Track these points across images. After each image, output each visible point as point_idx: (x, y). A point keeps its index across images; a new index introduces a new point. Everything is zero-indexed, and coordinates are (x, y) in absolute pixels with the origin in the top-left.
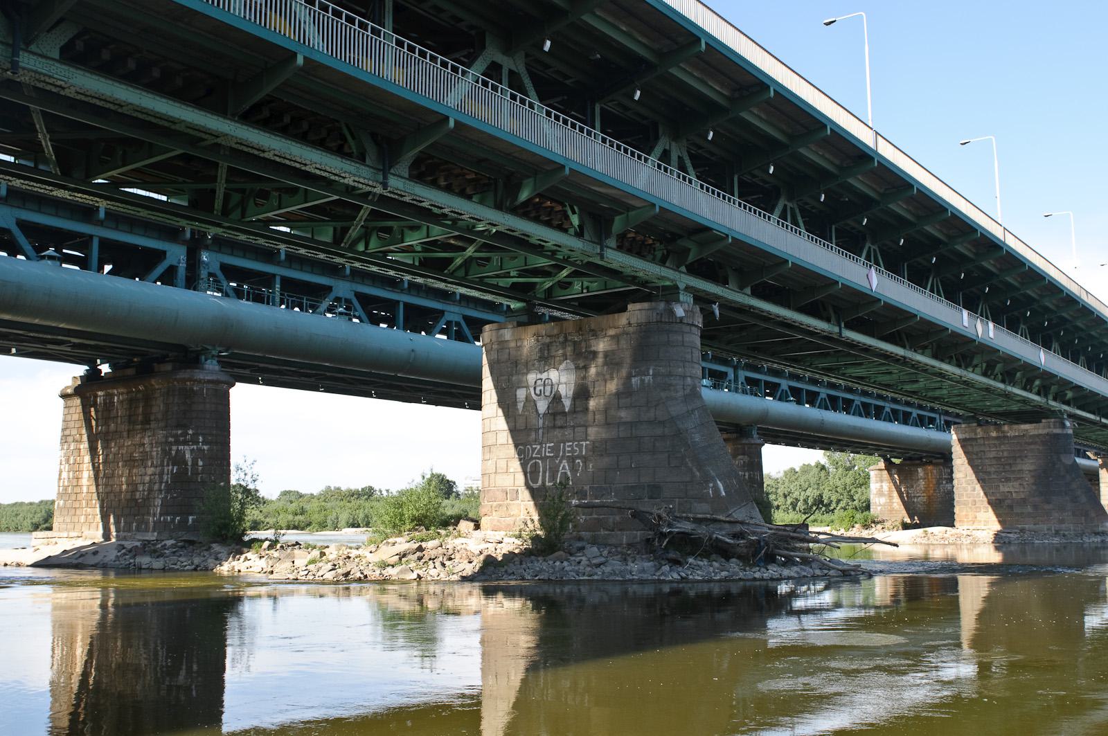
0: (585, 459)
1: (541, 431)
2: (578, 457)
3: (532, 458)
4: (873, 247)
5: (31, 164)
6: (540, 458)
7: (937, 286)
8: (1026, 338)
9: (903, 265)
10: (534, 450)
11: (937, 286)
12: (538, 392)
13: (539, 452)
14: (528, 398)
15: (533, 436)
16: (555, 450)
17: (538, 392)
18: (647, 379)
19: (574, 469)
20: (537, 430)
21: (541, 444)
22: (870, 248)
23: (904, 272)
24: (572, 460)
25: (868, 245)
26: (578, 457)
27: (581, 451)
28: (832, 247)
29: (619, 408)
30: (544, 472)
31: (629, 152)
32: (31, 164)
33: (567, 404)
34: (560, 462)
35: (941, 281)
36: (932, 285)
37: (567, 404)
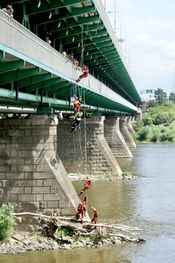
29: (25, 165)
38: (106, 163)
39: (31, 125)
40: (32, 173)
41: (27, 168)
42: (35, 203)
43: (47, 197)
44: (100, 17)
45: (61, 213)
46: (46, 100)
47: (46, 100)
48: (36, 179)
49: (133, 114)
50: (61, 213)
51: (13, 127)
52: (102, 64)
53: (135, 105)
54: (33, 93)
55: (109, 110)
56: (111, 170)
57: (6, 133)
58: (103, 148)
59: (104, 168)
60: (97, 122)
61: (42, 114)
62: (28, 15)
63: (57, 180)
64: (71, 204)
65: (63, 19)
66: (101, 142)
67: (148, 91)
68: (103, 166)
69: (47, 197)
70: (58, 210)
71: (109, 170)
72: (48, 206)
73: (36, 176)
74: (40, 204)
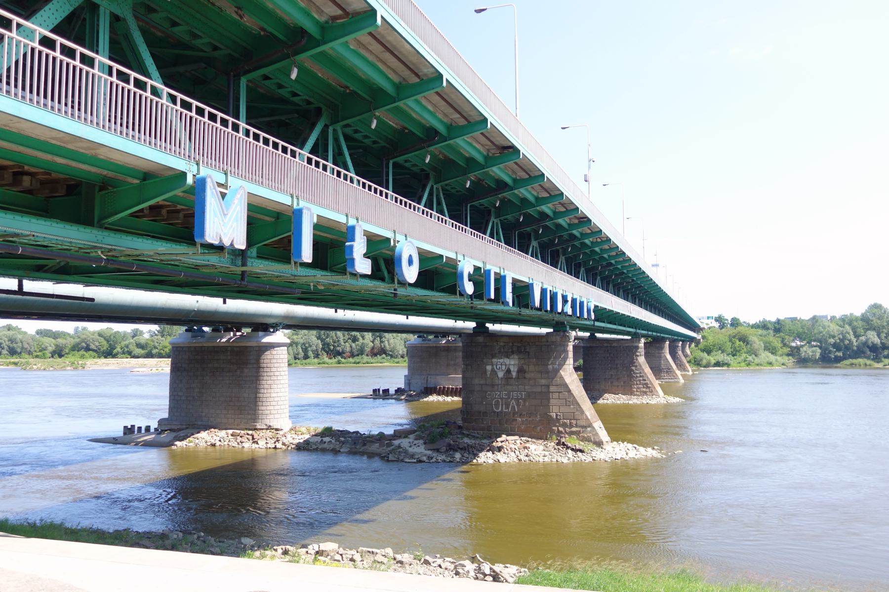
0: (524, 400)
1: (500, 386)
2: (521, 399)
3: (495, 398)
4: (496, 221)
5: (598, 335)
6: (500, 398)
7: (336, 140)
8: (499, 240)
9: (466, 207)
10: (496, 394)
11: (336, 140)
12: (498, 368)
13: (499, 395)
14: (493, 370)
15: (496, 387)
16: (508, 395)
17: (498, 368)
18: (555, 366)
19: (518, 405)
20: (498, 385)
21: (500, 392)
22: (493, 222)
23: (237, 100)
24: (517, 400)
25: (492, 219)
26: (521, 399)
27: (522, 396)
28: (446, 221)
29: (541, 378)
30: (502, 405)
31: (251, 135)
32: (598, 335)
33: (514, 374)
34: (511, 401)
35: (347, 138)
36: (431, 194)
37: (514, 374)
38: (646, 384)
39: (547, 341)
40: (548, 386)
41: (543, 382)
42: (551, 414)
43: (563, 409)
44: (160, 203)
45: (576, 425)
46: (638, 331)
47: (638, 331)
48: (552, 392)
49: (692, 340)
50: (576, 425)
51: (531, 344)
52: (636, 288)
53: (694, 332)
54: (633, 328)
55: (658, 334)
56: (652, 391)
57: (525, 349)
58: (643, 370)
59: (644, 390)
60: (636, 344)
61: (559, 331)
62: (537, 241)
63: (572, 394)
64: (587, 416)
65: (575, 243)
66: (641, 363)
67: (708, 318)
68: (644, 387)
69: (563, 409)
70: (574, 422)
71: (649, 392)
72: (565, 417)
73: (552, 389)
74: (557, 415)
